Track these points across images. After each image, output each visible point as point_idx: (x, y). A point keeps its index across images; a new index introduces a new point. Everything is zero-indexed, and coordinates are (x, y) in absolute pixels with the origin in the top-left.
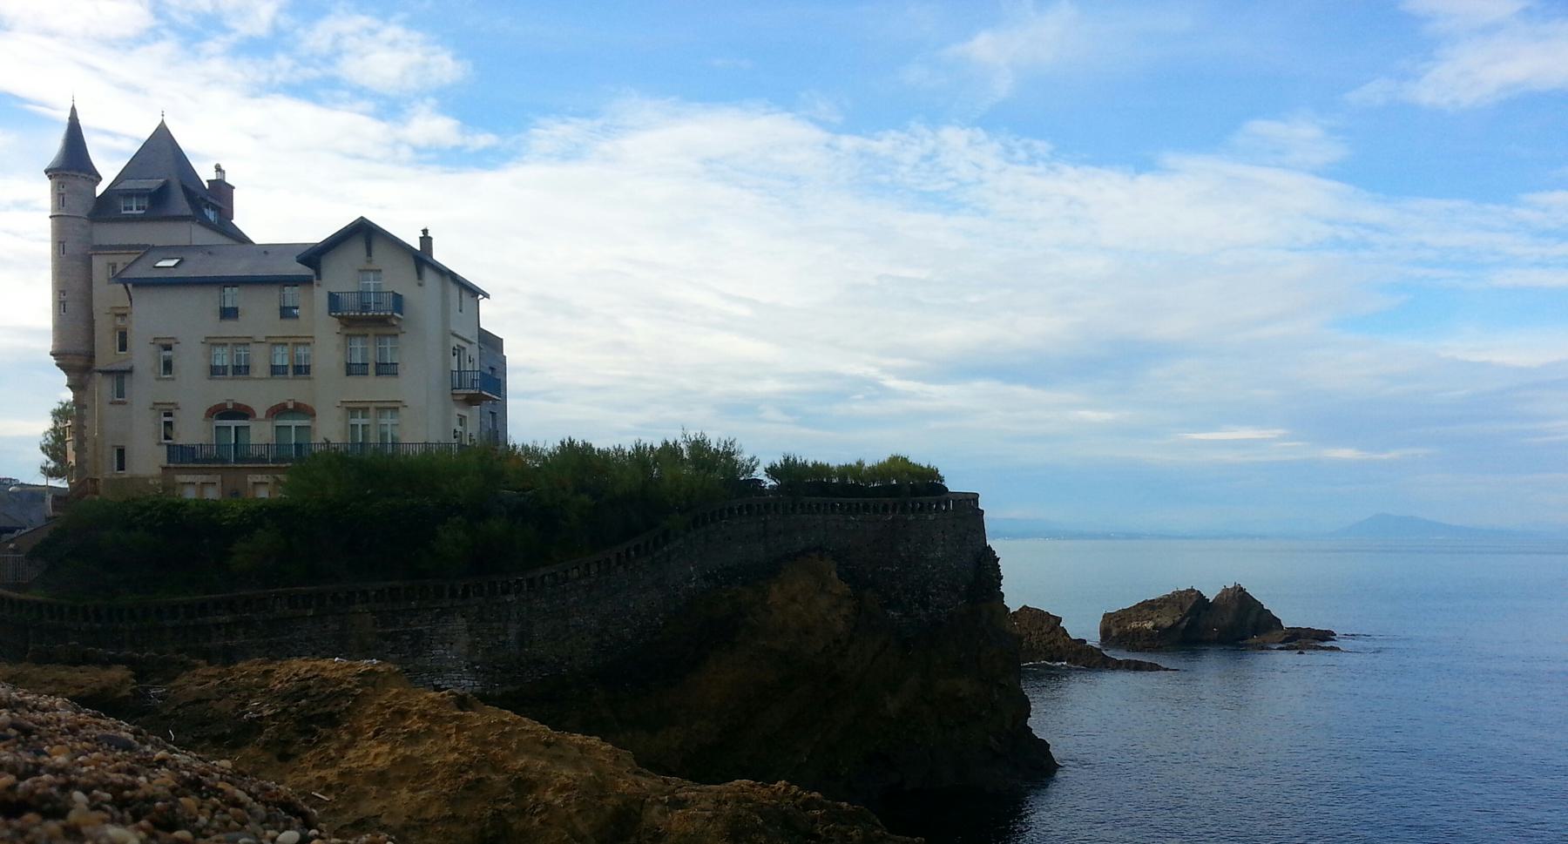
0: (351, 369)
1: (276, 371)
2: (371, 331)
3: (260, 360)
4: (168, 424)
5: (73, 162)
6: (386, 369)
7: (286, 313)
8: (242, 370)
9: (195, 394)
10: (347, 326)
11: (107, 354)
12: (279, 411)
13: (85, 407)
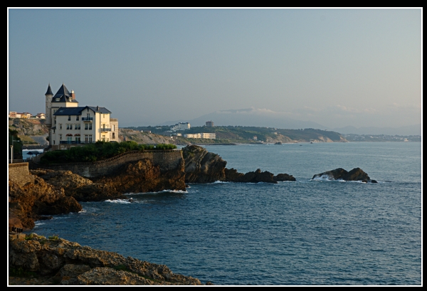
3: (74, 127)
5: (49, 92)
7: (69, 120)
9: (65, 132)
11: (53, 126)
12: (76, 135)
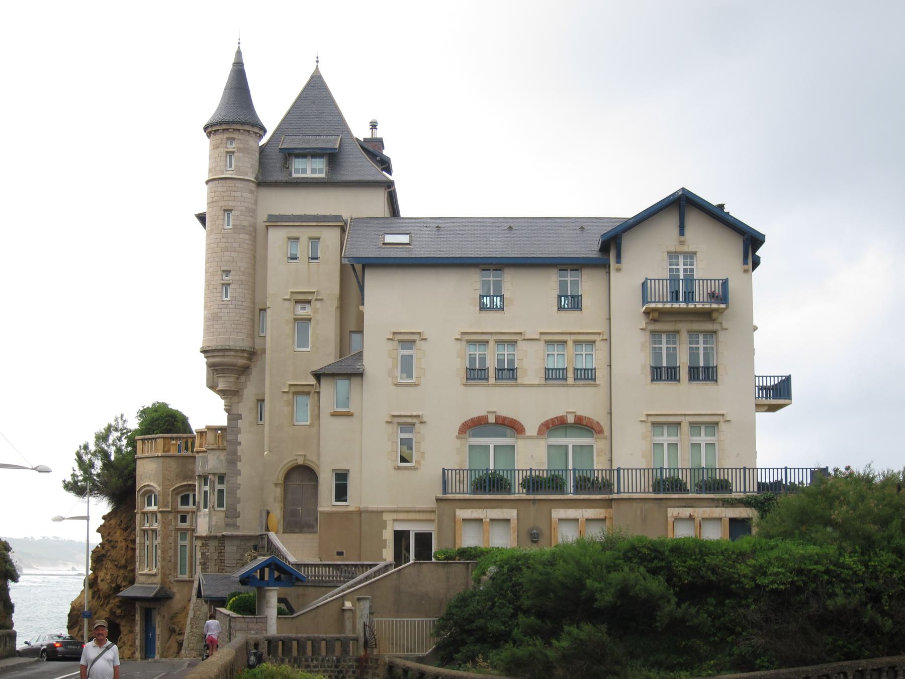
0: (663, 373)
1: (554, 376)
2: (684, 327)
3: (531, 360)
4: (407, 443)
5: (235, 116)
6: (704, 373)
8: (508, 373)
10: (654, 320)
13: (239, 417)
